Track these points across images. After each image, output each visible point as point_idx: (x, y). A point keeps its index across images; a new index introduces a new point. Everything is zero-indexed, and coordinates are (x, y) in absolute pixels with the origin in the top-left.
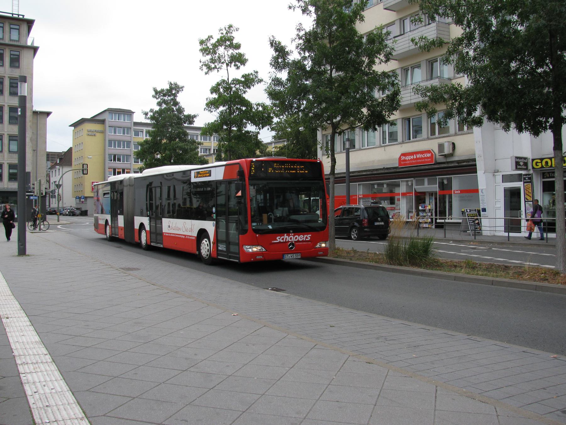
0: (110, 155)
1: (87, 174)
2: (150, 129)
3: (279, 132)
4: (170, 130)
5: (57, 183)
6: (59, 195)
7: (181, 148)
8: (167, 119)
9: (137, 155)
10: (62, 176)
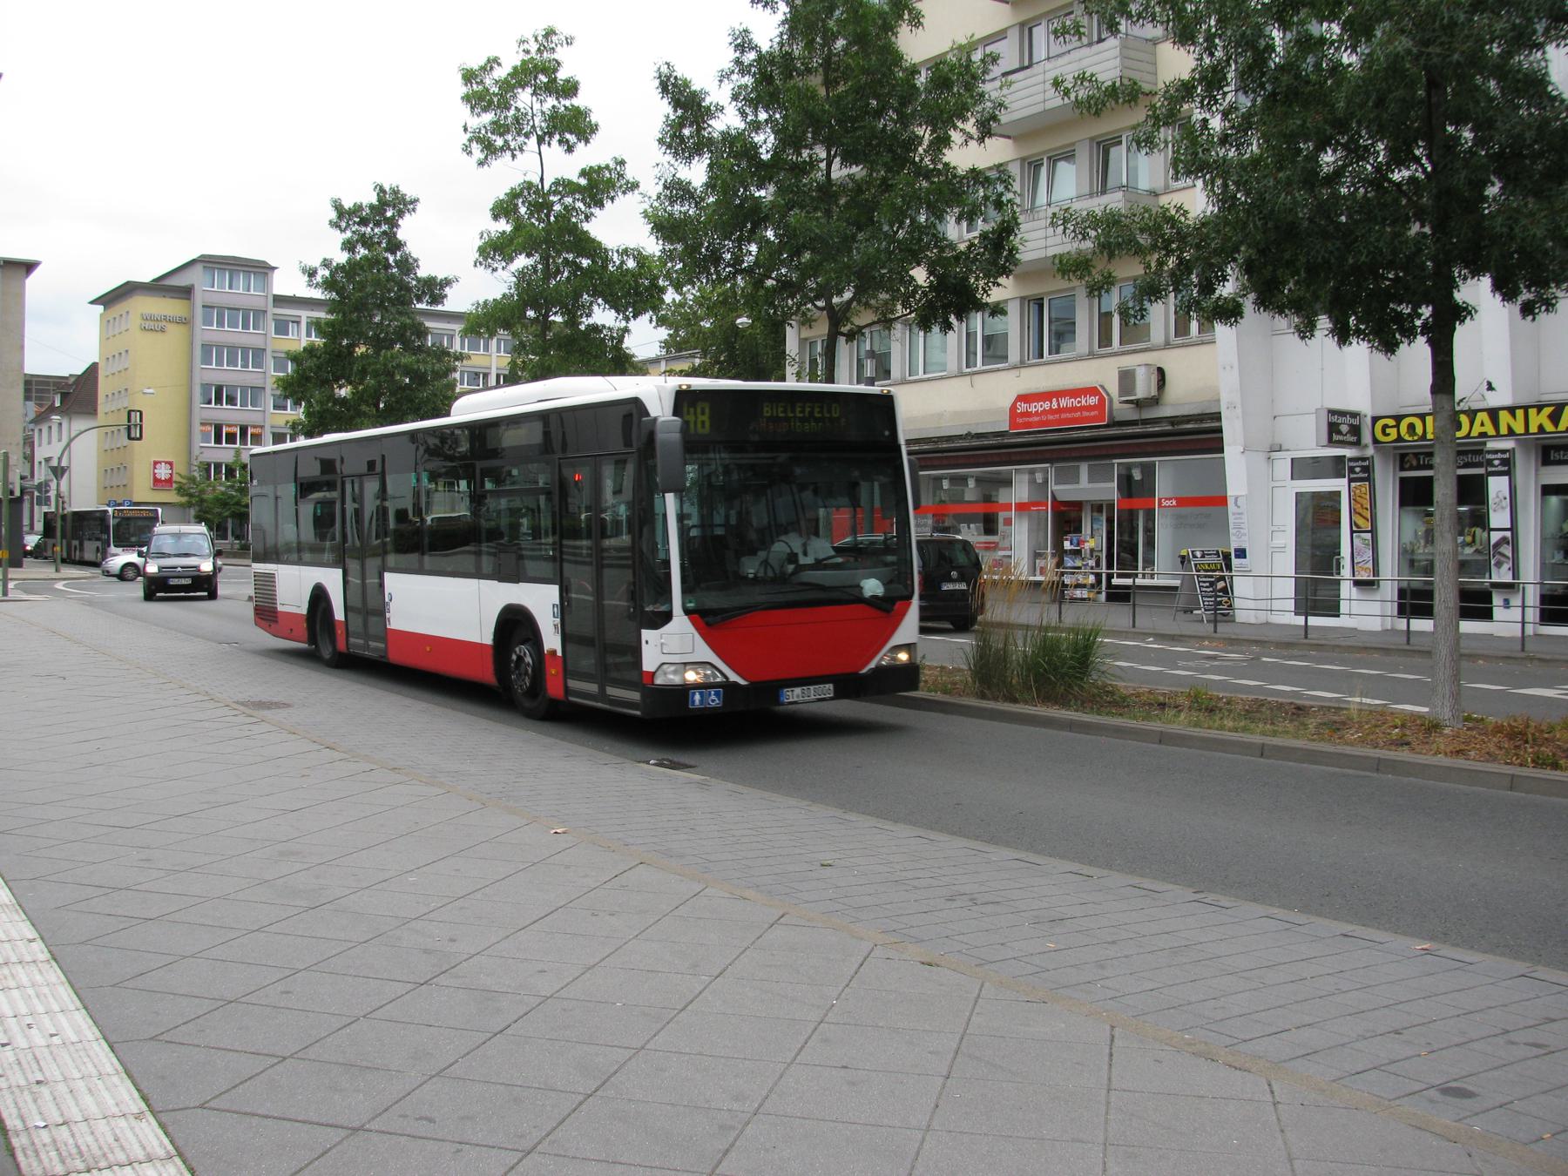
0: (206, 387)
1: (140, 438)
2: (321, 315)
3: (677, 331)
4: (377, 319)
5: (55, 463)
6: (58, 496)
7: (407, 371)
8: (369, 289)
9: (285, 389)
10: (68, 445)
